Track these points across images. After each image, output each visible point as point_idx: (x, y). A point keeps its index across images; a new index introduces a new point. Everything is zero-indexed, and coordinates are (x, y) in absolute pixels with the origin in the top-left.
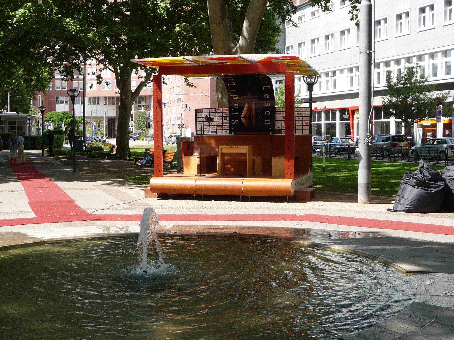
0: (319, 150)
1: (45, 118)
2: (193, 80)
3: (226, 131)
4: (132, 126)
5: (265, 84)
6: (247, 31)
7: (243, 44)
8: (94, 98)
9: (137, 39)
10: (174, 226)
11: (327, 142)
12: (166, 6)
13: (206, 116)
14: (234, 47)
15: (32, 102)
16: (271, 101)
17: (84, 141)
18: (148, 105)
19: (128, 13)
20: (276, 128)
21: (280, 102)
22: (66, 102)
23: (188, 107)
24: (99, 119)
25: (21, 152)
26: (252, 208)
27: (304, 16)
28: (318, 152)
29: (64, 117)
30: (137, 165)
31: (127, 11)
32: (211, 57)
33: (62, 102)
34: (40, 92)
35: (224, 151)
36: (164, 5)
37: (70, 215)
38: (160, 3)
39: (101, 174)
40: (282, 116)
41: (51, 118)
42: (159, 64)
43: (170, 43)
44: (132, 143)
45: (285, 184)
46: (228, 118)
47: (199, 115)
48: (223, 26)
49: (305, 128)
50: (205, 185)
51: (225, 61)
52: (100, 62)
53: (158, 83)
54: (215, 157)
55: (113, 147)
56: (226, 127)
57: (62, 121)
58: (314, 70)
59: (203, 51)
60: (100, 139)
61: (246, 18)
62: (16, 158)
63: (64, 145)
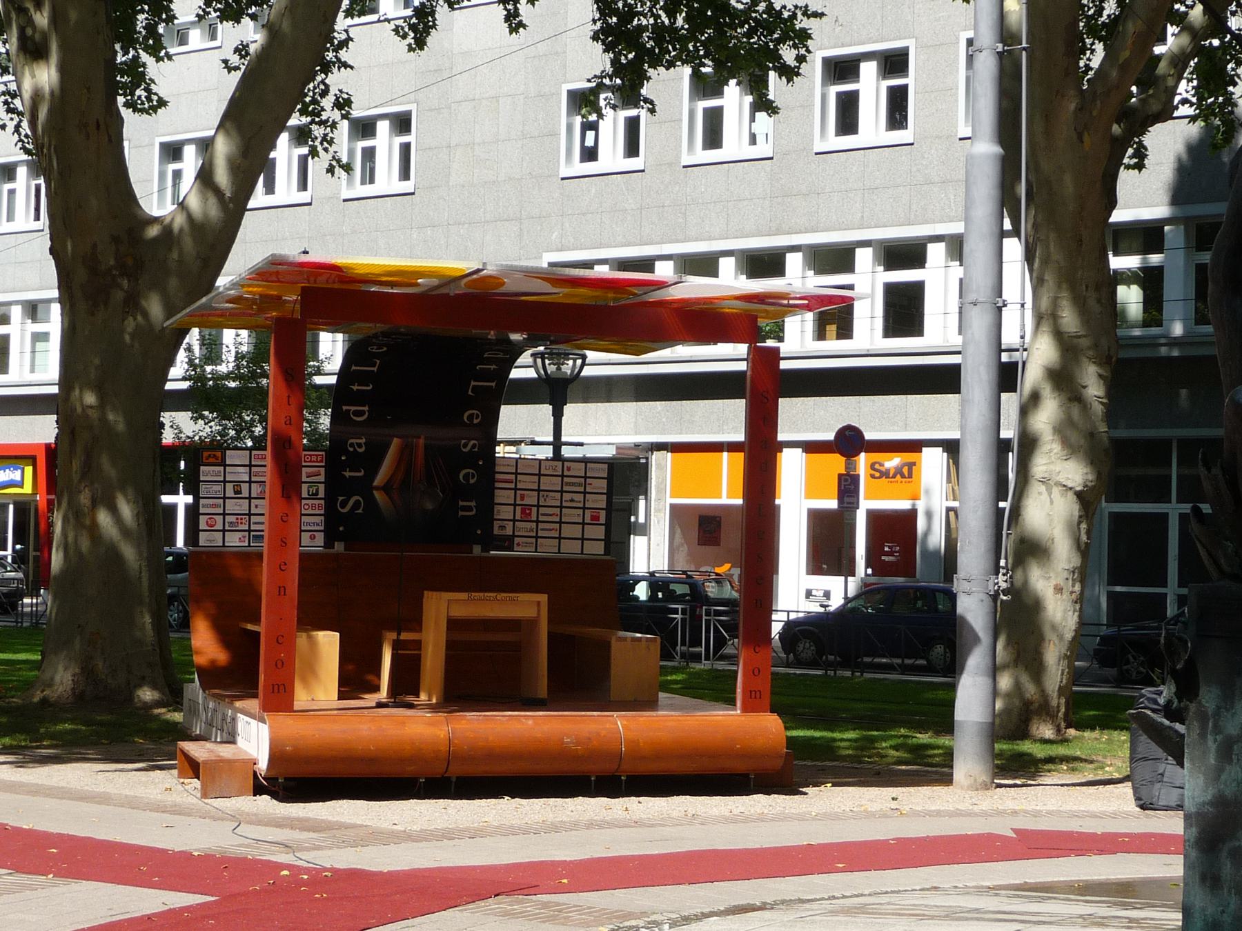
46: (322, 488)
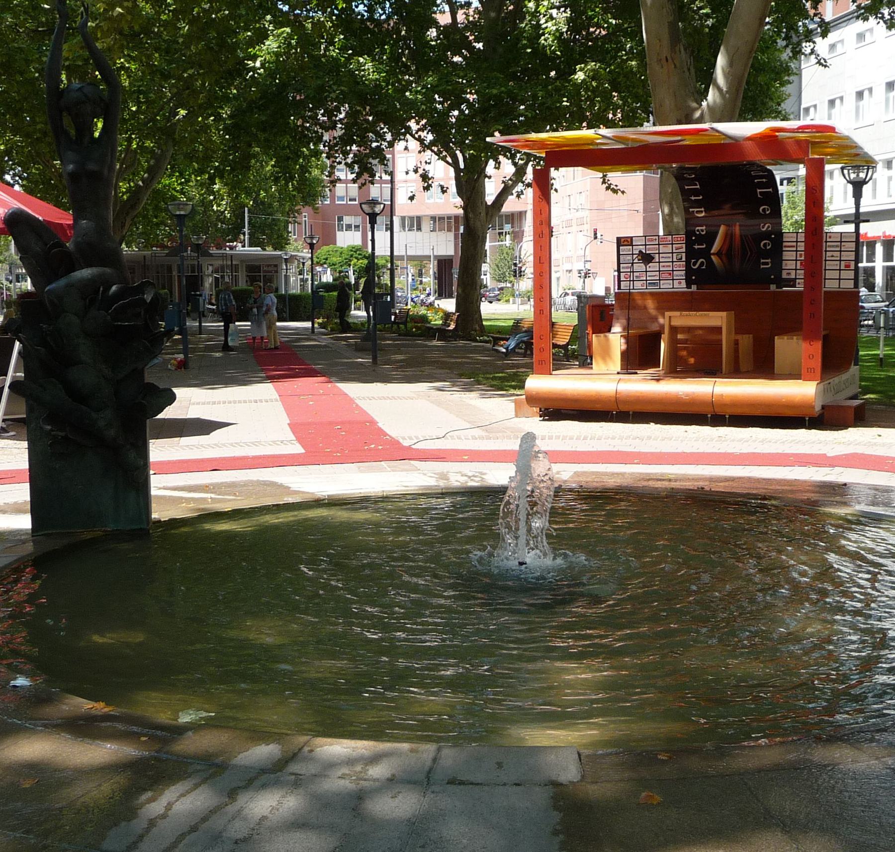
0: (870, 322)
1: (315, 260)
2: (616, 177)
3: (680, 283)
4: (487, 275)
5: (761, 185)
6: (726, 75)
7: (715, 102)
8: (411, 218)
9: (498, 98)
10: (576, 474)
11: (887, 306)
12: (557, 30)
13: (640, 251)
14: (697, 109)
15: (290, 228)
16: (774, 221)
17: (392, 304)
18: (517, 232)
19: (480, 46)
20: (784, 276)
21: (789, 222)
22: (357, 227)
23: (599, 235)
24: (420, 261)
25: (271, 326)
26: (733, 441)
27: (842, 41)
28: (868, 326)
29: (352, 256)
30: (497, 351)
31: (477, 40)
32: (650, 131)
33: (349, 227)
34: (307, 207)
35: (676, 322)
36: (554, 28)
37: (370, 450)
38: (546, 22)
39: (427, 370)
40: (797, 251)
41: (326, 259)
42: (541, 144)
43: (565, 103)
44: (486, 309)
45: (803, 391)
47: (623, 251)
48: (675, 67)
49: (844, 274)
50: (637, 392)
51: (679, 138)
52: (425, 147)
53: (543, 186)
54: (656, 337)
55: (447, 316)
56: (681, 274)
57: (350, 265)
58: (866, 153)
59: (631, 120)
60: (422, 300)
61: (722, 48)
62: (262, 338)
63: (352, 312)
